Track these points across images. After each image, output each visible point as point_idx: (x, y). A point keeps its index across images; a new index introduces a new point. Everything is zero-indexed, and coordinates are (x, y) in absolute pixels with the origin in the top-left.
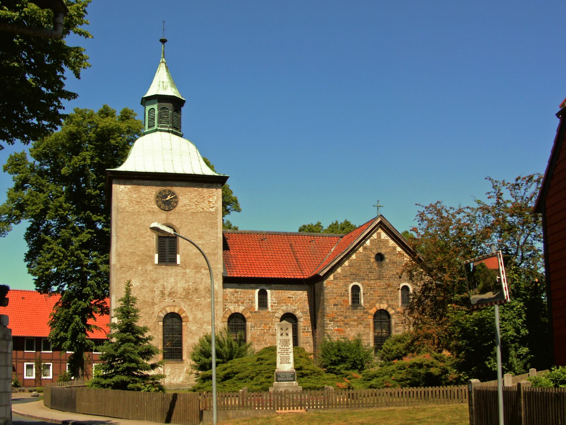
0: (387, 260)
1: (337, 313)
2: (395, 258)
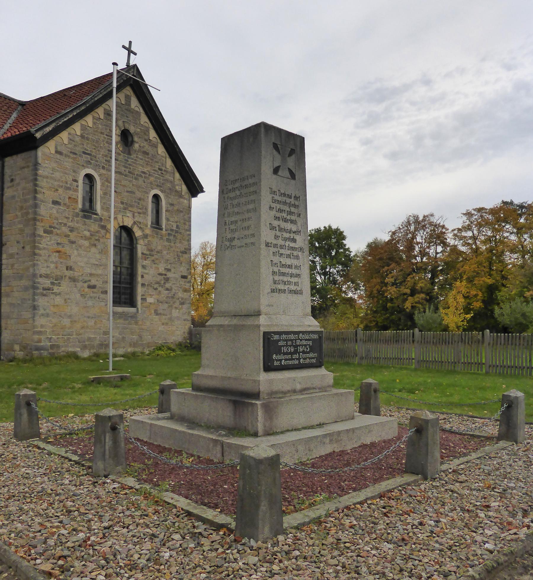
0: (136, 146)
1: (57, 219)
2: (147, 148)
